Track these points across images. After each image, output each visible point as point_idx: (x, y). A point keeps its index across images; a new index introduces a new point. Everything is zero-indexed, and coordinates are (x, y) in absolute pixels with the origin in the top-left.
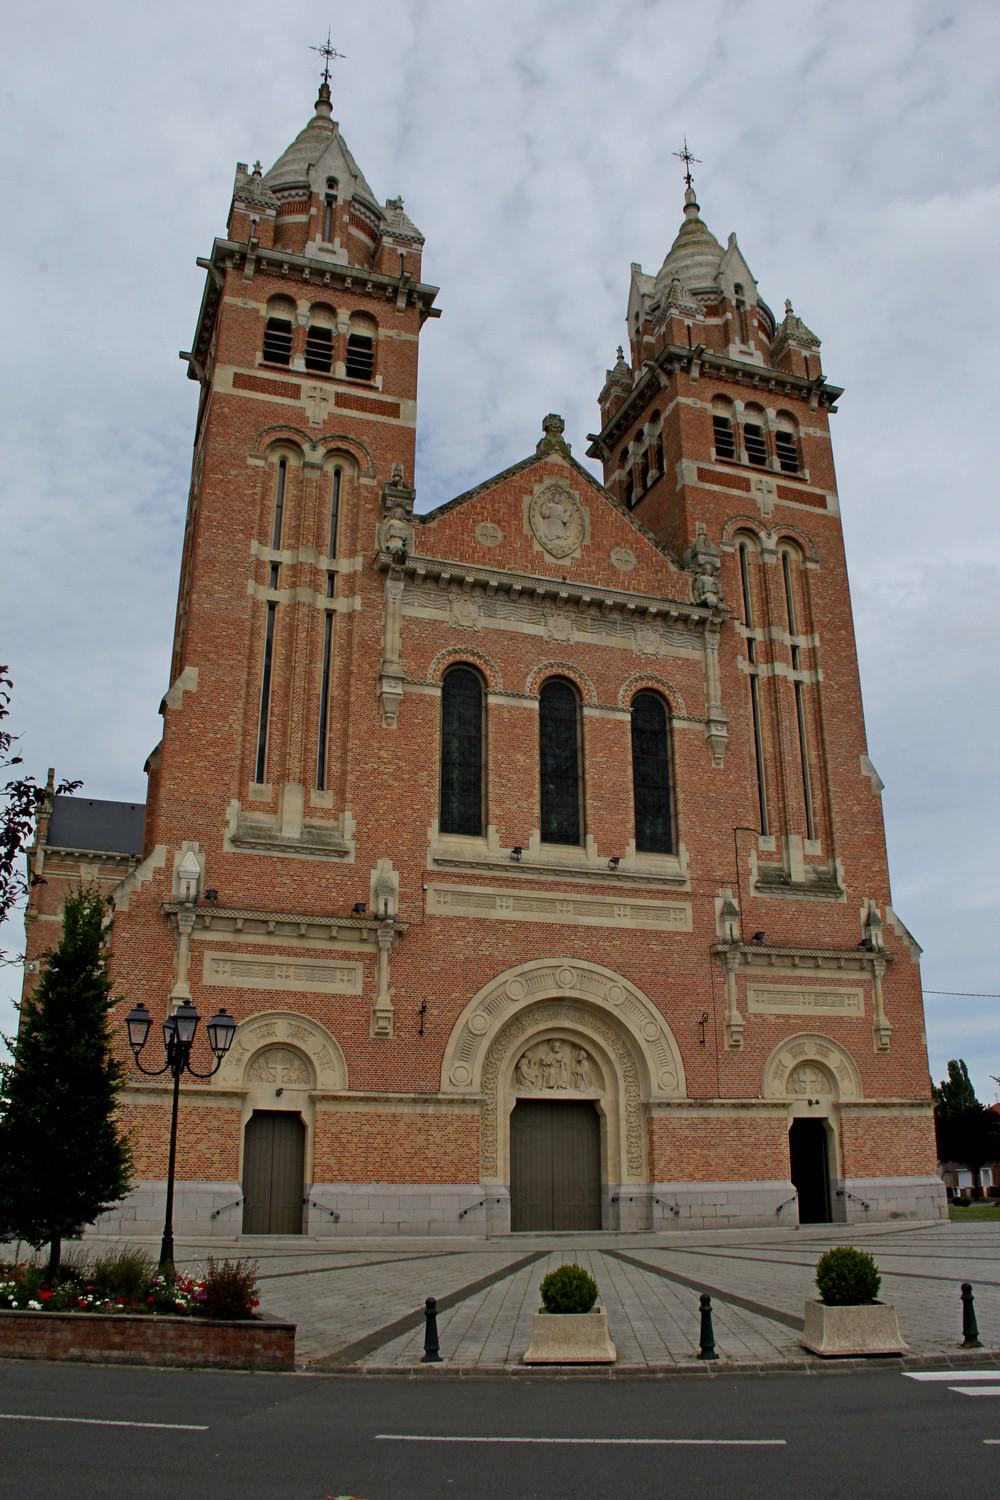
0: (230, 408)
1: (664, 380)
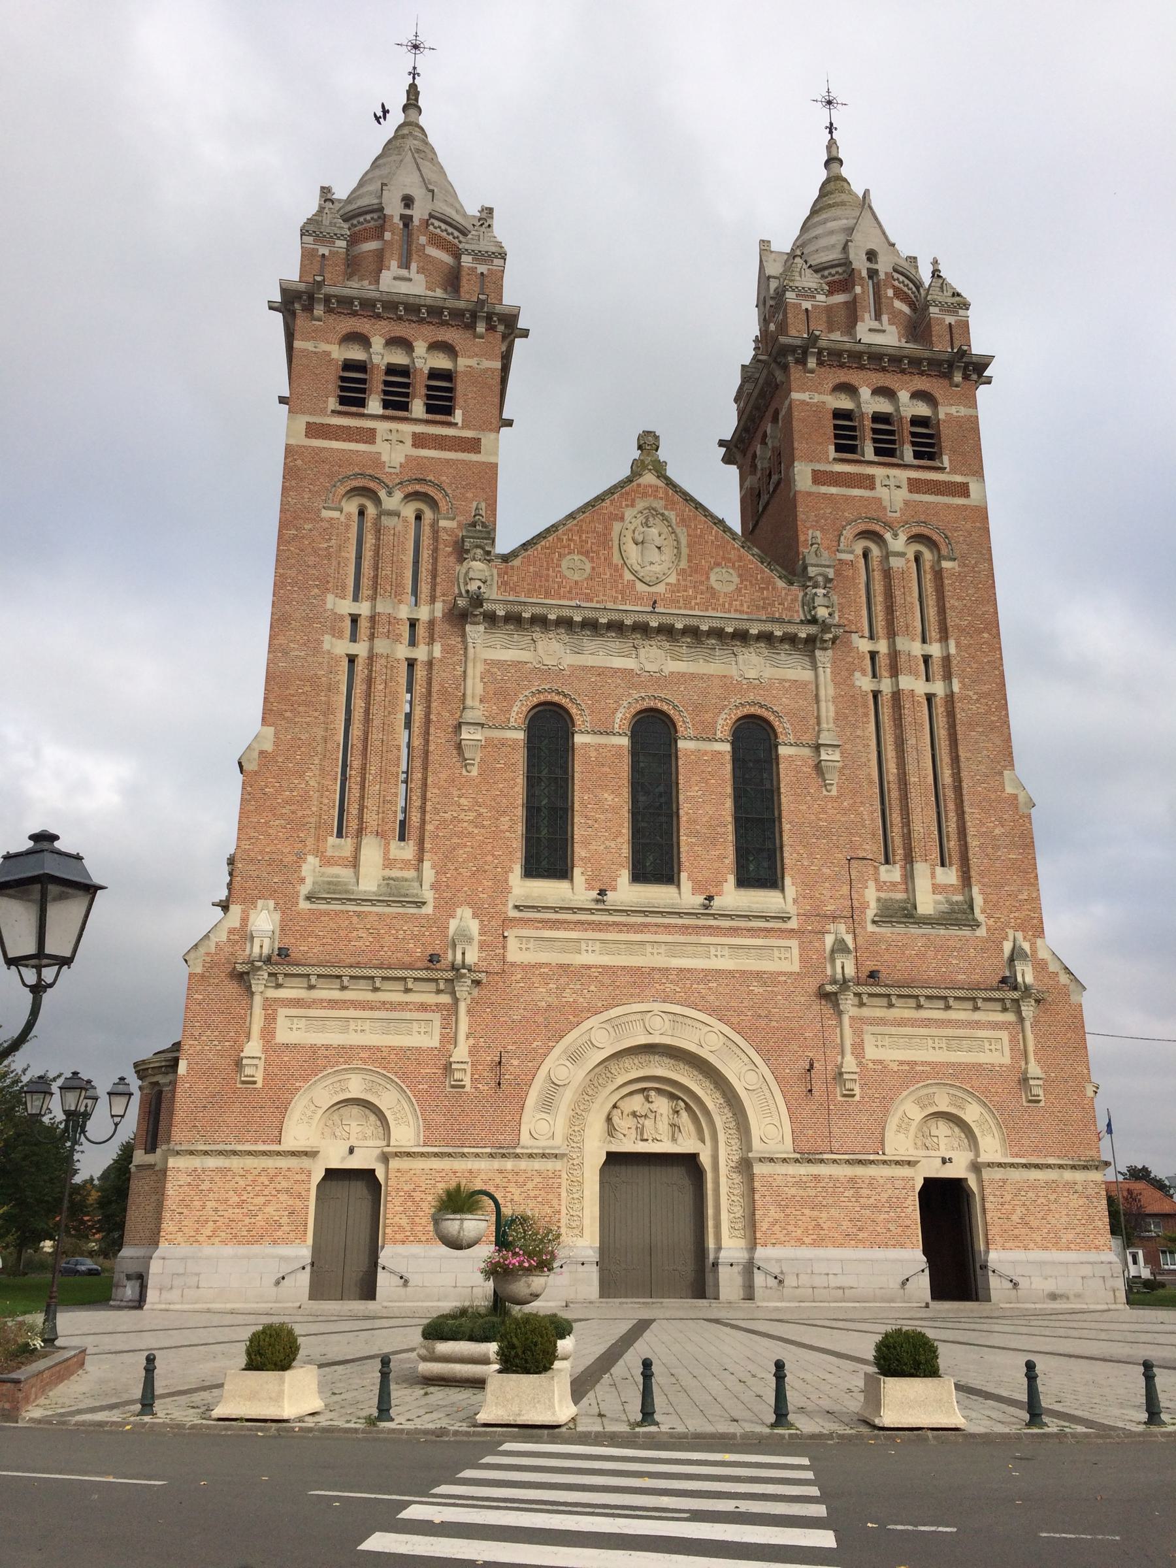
0: (303, 460)
1: (779, 376)
